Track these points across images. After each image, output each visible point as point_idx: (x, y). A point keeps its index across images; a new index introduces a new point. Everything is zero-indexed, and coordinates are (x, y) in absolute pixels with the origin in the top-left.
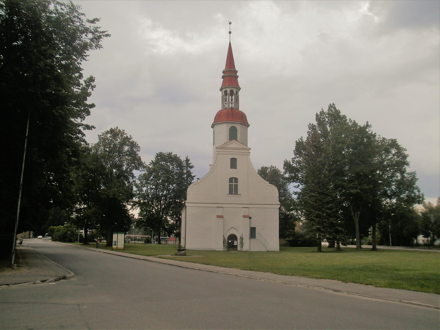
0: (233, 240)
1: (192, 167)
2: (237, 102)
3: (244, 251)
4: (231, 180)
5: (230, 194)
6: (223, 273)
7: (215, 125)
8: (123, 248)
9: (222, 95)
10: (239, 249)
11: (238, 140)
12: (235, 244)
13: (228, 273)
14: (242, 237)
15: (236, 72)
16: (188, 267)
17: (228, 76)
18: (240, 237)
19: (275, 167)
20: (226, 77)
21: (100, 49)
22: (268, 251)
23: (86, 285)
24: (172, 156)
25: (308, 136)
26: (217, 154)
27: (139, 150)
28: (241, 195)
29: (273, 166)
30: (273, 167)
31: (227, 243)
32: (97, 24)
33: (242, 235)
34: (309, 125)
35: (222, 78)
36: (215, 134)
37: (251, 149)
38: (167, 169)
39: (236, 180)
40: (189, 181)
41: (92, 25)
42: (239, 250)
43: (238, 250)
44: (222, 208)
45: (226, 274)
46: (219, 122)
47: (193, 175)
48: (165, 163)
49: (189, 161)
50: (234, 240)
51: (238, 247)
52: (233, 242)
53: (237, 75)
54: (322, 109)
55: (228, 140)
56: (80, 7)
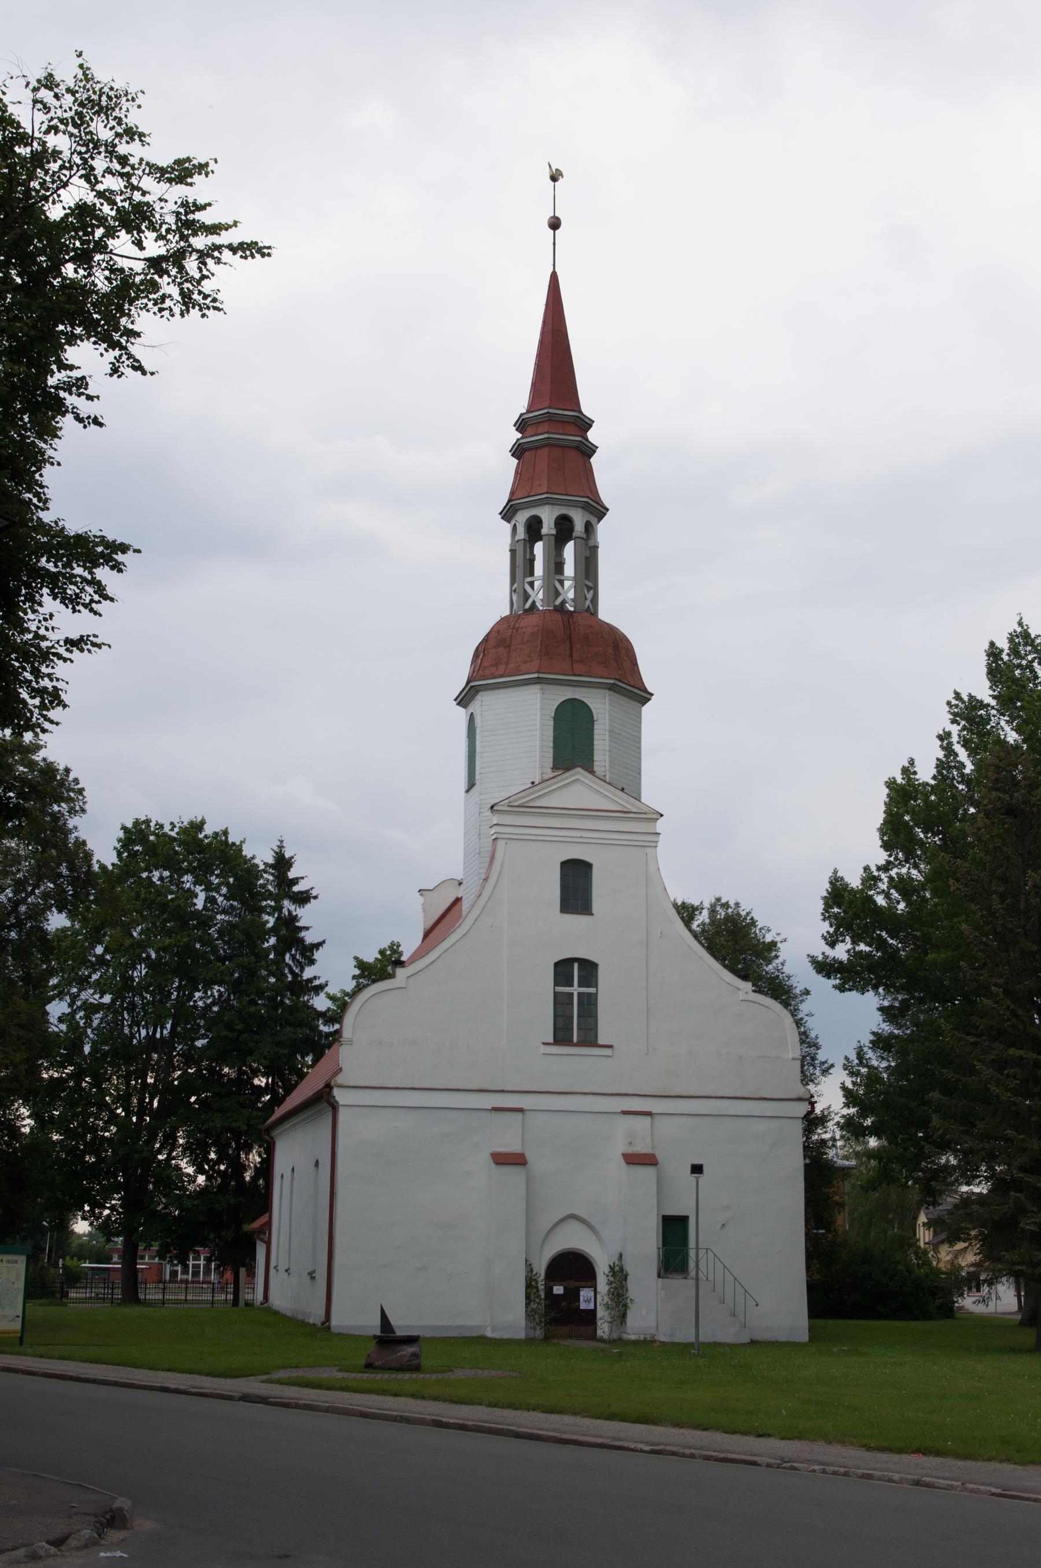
0: (573, 1284)
1: (303, 898)
2: (588, 580)
3: (635, 1343)
4: (563, 970)
5: (557, 1041)
6: (824, 1472)
7: (477, 692)
8: (20, 1335)
9: (514, 541)
10: (603, 1329)
11: (595, 768)
12: (588, 1301)
13: (832, 1468)
14: (622, 1269)
15: (585, 424)
16: (574, 1437)
17: (548, 444)
18: (612, 1268)
19: (737, 904)
20: (536, 448)
21: (203, 316)
22: (753, 1342)
23: (287, 1556)
24: (206, 837)
25: (941, 754)
26: (496, 839)
27: (77, 808)
28: (611, 1047)
29: (723, 901)
30: (726, 905)
31: (543, 1296)
32: (199, 189)
33: (621, 1255)
34: (954, 702)
35: (513, 455)
36: (478, 737)
37: (662, 815)
38: (179, 906)
39: (589, 969)
40: (292, 971)
41: (177, 193)
42: (606, 1336)
43: (599, 1333)
44: (518, 1116)
45: (846, 1474)
46: (501, 676)
47: (309, 937)
48: (166, 873)
49: (291, 866)
50: (577, 1284)
51: (599, 1323)
52: (573, 1295)
53: (590, 439)
54: (1020, 624)
55: (549, 770)
56: (133, 100)
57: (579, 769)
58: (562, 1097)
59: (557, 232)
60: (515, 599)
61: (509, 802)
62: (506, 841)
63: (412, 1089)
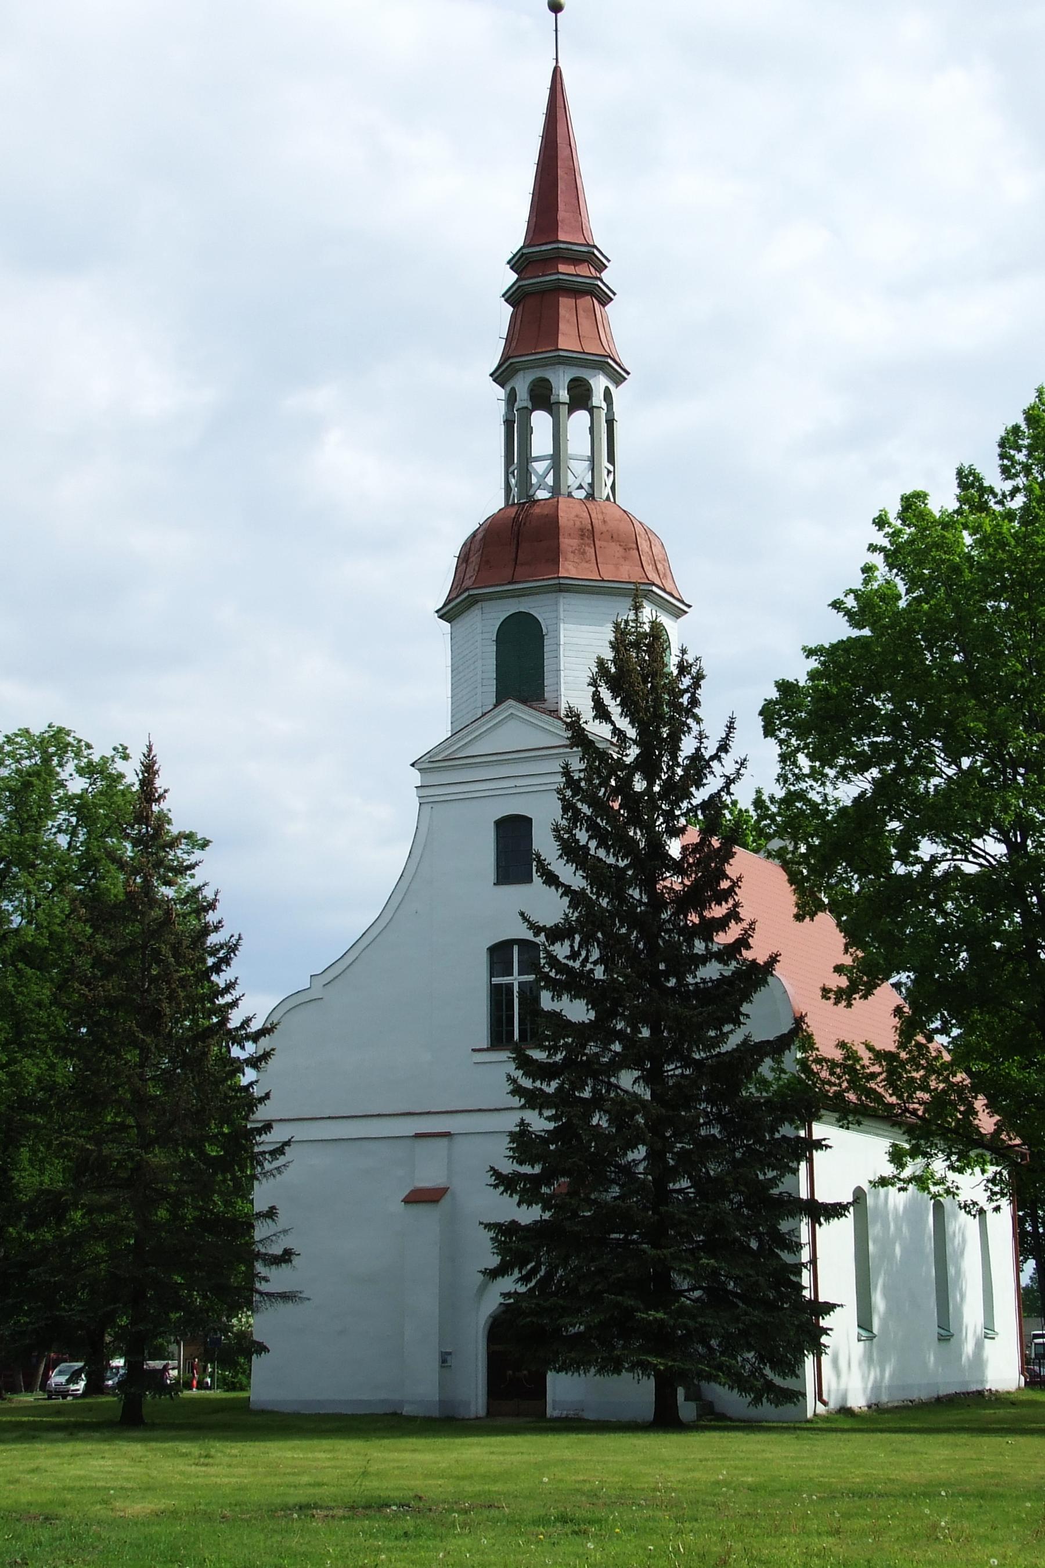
44: (444, 1142)
57: (511, 702)
58: (496, 1114)
59: (559, 15)
60: (513, 481)
61: (430, 757)
62: (431, 805)
63: (379, 1115)
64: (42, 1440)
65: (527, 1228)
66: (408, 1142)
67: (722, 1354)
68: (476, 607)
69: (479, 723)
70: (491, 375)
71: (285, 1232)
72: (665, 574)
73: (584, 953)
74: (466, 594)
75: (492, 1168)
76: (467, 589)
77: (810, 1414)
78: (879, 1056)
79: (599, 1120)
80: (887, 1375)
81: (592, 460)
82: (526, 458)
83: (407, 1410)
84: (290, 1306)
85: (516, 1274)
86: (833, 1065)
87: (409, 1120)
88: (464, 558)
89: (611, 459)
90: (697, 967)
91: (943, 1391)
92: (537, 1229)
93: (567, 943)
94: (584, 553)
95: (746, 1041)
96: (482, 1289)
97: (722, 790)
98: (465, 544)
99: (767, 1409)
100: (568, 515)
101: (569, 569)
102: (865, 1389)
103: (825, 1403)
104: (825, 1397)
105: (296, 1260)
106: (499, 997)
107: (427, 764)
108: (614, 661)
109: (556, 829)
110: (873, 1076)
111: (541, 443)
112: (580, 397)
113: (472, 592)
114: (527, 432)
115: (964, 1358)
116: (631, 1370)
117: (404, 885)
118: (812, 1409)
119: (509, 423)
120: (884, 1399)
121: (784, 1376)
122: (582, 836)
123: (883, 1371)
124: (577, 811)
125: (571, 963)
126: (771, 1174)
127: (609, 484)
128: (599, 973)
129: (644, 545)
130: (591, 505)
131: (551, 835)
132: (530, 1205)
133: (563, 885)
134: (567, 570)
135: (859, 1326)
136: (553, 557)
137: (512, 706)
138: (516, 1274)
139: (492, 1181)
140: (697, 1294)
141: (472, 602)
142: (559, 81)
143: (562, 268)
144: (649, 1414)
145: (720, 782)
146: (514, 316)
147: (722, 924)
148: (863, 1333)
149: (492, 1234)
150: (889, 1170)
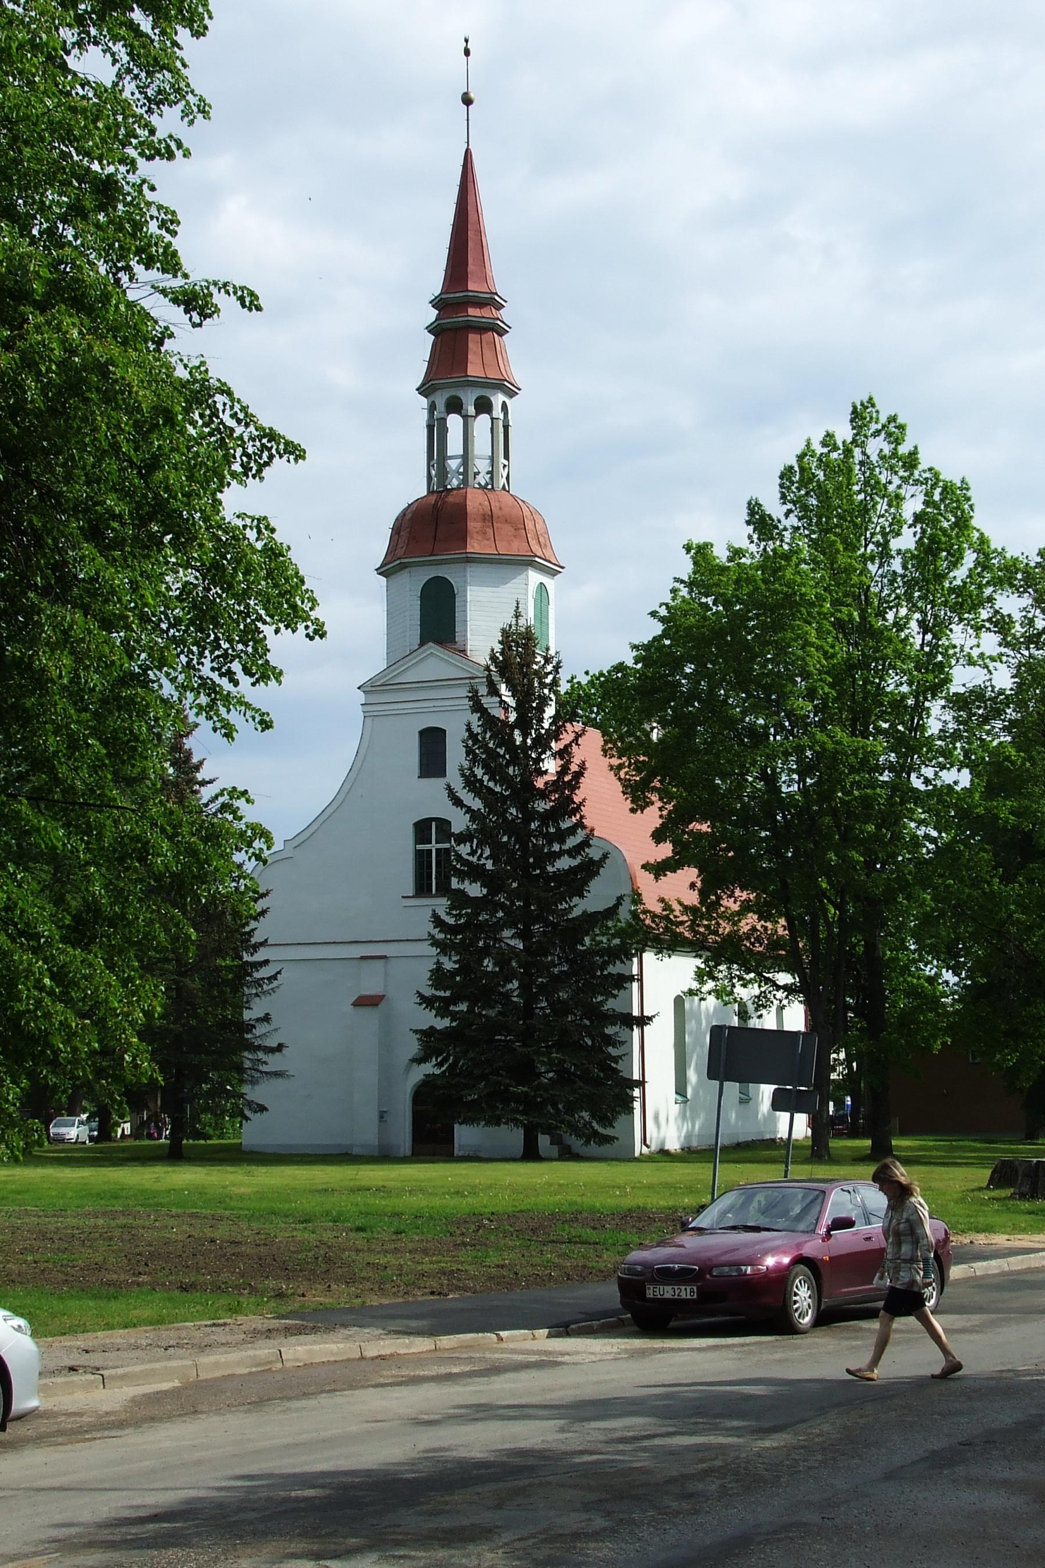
44: (382, 961)
57: (431, 644)
60: (433, 473)
64: (126, 1165)
65: (440, 1032)
66: (356, 962)
67: (565, 1113)
68: (407, 570)
69: (407, 659)
70: (417, 389)
71: (276, 1030)
72: (545, 545)
73: (479, 851)
74: (398, 562)
75: (418, 992)
76: (399, 559)
77: (637, 1154)
78: (686, 909)
79: (488, 964)
80: (697, 1127)
81: (492, 459)
82: (443, 457)
83: (356, 1151)
84: (280, 1080)
85: (434, 1062)
86: (654, 916)
87: (353, 947)
88: (397, 530)
89: (507, 457)
90: (555, 861)
91: (741, 1140)
92: (447, 1033)
93: (468, 844)
94: (485, 533)
95: (585, 912)
96: (408, 1069)
97: (573, 741)
98: (397, 519)
99: (593, 1148)
100: (475, 501)
101: (474, 546)
102: (679, 1137)
103: (648, 1146)
104: (648, 1142)
105: (285, 1051)
106: (422, 859)
107: (370, 688)
108: (502, 653)
109: (462, 769)
110: (682, 923)
111: (454, 445)
112: (484, 406)
113: (403, 561)
114: (444, 430)
115: (760, 1116)
116: (506, 1123)
117: (353, 775)
118: (638, 1149)
119: (430, 428)
120: (694, 1144)
121: (605, 1126)
122: (479, 772)
123: (693, 1126)
124: (475, 755)
125: (470, 858)
126: (600, 998)
127: (505, 475)
128: (489, 865)
129: (529, 525)
130: (491, 495)
131: (458, 773)
132: (442, 1018)
133: (466, 806)
134: (473, 547)
135: (676, 1093)
136: (462, 537)
137: (432, 648)
138: (434, 1062)
139: (418, 1000)
140: (551, 1075)
141: (403, 567)
142: (469, 171)
143: (472, 311)
144: (520, 1151)
145: (572, 736)
146: (434, 345)
147: (572, 831)
148: (680, 1098)
149: (418, 1036)
150: (695, 985)
